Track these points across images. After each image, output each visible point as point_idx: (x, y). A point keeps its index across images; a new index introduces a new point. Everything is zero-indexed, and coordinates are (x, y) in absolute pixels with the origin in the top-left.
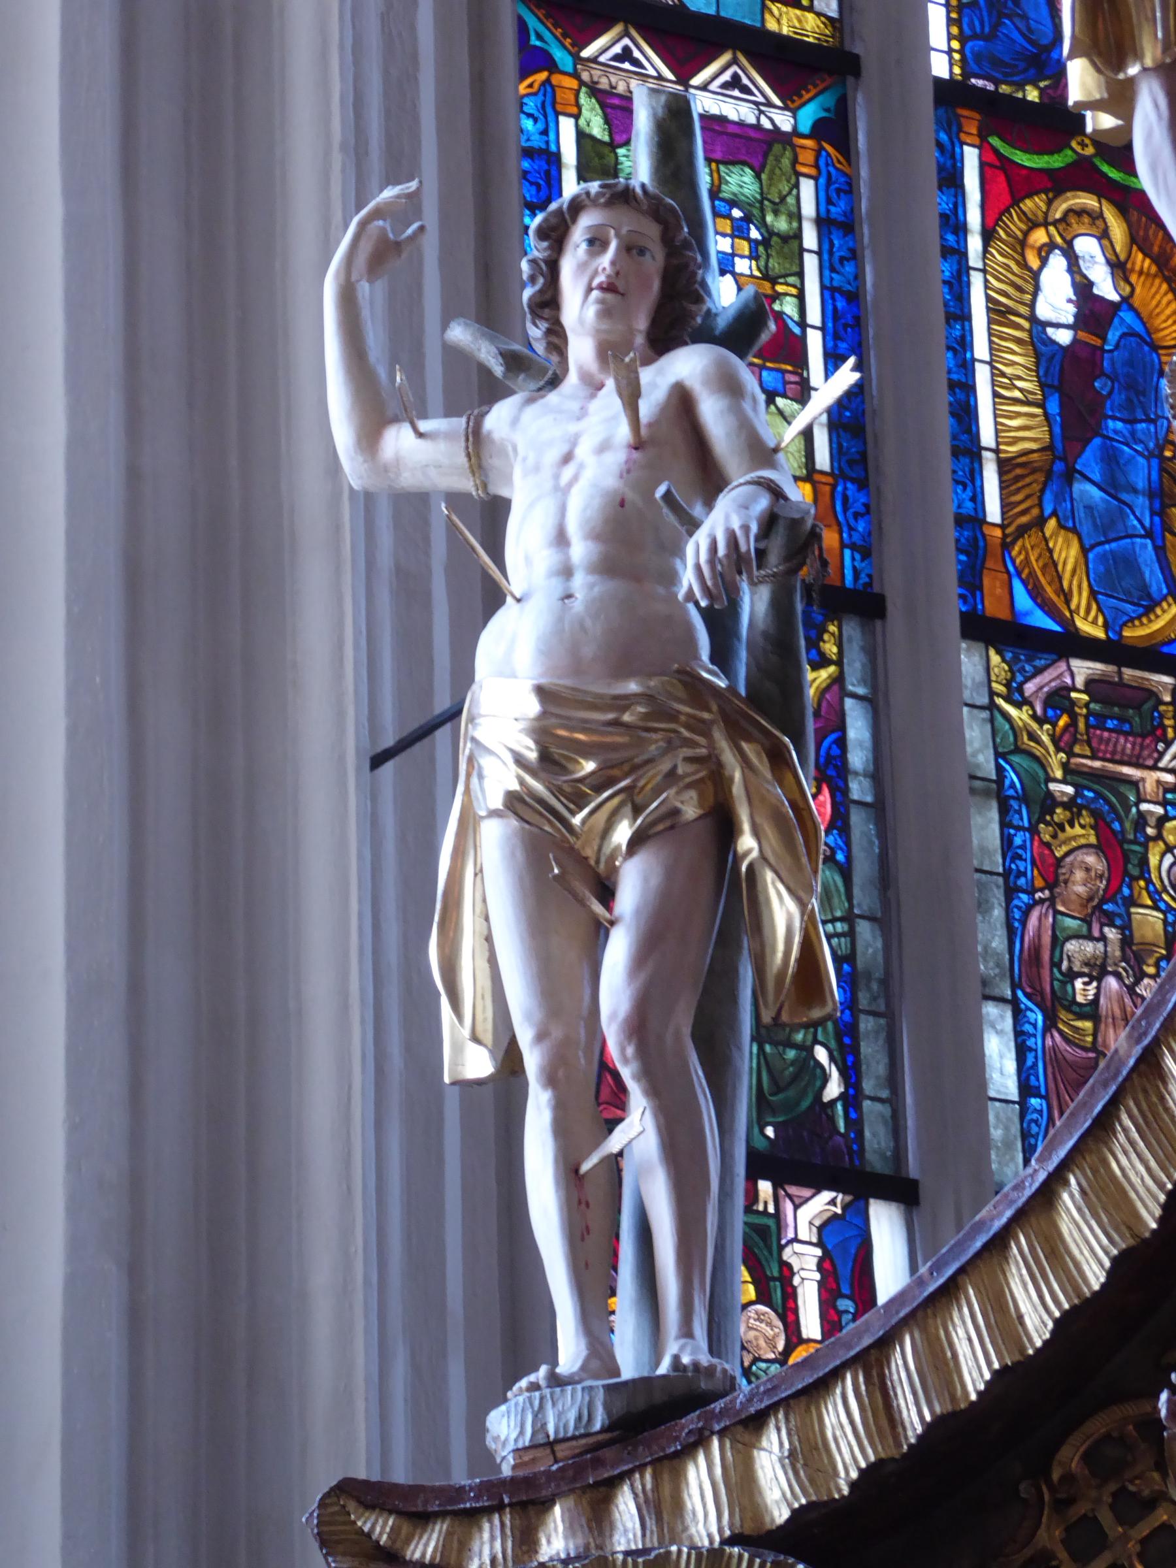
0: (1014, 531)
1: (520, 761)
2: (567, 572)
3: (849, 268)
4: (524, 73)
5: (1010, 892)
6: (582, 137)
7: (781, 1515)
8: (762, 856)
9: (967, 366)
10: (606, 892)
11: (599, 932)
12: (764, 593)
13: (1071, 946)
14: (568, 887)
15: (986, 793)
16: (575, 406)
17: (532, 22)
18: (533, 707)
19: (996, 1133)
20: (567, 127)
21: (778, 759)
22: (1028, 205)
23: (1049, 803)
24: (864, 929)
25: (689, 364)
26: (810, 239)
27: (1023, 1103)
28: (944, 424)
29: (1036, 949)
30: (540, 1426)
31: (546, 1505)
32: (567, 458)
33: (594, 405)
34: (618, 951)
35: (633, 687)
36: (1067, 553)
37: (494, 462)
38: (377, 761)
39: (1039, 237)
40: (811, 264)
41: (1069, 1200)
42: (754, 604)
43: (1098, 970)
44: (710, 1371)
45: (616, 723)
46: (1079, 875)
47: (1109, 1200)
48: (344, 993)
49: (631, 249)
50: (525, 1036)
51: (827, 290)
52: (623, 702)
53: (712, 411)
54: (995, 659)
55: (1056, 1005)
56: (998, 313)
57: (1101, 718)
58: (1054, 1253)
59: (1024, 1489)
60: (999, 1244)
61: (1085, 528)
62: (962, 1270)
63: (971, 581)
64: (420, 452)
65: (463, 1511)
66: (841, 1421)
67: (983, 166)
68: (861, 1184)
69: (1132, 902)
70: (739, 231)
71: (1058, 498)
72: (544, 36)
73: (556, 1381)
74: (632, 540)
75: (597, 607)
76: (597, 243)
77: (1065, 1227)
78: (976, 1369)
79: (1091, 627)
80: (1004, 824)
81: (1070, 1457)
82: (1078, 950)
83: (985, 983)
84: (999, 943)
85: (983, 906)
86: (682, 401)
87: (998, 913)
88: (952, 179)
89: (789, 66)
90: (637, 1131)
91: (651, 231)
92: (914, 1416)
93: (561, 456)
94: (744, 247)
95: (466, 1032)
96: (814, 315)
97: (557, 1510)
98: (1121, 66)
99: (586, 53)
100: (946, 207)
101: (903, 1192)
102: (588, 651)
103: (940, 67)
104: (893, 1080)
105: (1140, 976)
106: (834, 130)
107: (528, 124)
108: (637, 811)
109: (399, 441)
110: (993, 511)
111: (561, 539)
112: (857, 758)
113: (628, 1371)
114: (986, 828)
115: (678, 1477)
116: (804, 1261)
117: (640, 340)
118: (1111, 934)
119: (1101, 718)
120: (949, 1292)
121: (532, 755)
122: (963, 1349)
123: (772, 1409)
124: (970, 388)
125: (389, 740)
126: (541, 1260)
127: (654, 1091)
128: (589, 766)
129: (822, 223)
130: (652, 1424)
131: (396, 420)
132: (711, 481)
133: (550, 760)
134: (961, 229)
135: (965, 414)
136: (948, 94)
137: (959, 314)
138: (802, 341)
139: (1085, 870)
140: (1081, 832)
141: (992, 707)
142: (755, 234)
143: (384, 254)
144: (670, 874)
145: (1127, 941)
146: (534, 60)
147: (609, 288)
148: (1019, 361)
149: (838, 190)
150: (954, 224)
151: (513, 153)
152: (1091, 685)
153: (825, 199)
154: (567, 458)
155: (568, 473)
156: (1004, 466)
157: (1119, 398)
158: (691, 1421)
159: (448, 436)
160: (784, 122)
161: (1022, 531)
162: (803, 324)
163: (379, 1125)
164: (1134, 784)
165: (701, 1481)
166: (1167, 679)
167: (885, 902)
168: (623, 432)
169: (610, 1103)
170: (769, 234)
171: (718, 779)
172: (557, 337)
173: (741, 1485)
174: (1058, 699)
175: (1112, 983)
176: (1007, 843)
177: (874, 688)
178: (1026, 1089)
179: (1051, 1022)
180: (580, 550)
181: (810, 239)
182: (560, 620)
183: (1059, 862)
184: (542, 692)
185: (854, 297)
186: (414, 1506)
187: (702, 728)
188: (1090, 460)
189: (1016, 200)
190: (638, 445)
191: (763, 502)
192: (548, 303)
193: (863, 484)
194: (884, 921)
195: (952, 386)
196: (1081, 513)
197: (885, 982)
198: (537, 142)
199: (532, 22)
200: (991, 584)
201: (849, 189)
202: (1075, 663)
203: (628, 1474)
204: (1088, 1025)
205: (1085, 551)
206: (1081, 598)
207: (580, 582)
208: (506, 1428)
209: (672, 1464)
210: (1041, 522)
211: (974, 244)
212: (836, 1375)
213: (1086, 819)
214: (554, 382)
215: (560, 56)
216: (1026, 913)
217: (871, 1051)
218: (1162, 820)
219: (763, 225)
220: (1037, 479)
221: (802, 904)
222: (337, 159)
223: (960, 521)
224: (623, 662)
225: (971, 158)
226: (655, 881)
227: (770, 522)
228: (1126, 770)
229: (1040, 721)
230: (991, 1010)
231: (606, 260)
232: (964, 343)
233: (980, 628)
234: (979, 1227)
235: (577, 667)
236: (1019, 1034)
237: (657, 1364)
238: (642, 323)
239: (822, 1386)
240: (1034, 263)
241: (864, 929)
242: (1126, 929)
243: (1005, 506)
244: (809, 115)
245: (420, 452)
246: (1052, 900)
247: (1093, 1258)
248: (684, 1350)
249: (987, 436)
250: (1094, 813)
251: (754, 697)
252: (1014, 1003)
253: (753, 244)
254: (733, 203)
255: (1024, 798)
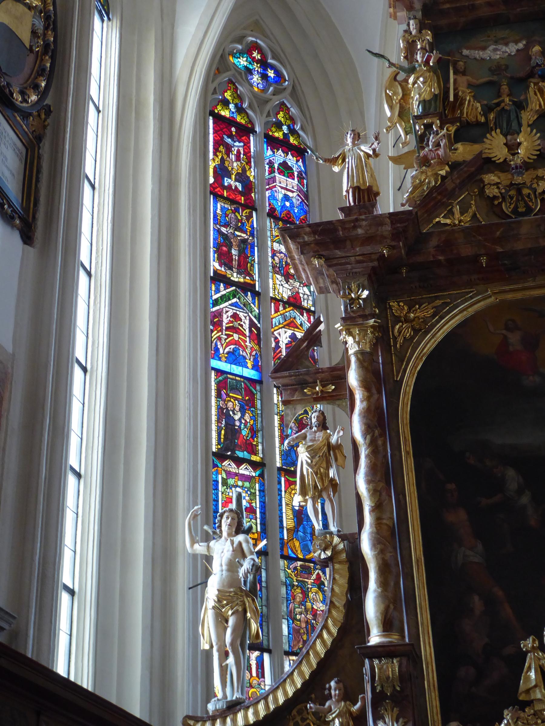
0: (289, 541)
1: (215, 601)
2: (222, 571)
3: (264, 498)
4: (214, 468)
5: (287, 601)
6: (222, 478)
7: (252, 722)
8: (251, 617)
9: (282, 513)
10: (227, 621)
11: (225, 629)
12: (252, 576)
13: (297, 610)
14: (221, 620)
15: (284, 584)
16: (223, 543)
17: (215, 460)
18: (217, 593)
19: (284, 641)
20: (220, 476)
21: (253, 600)
22: (292, 487)
23: (293, 586)
24: (264, 607)
25: (241, 538)
26: (257, 493)
27: (288, 636)
28: (278, 523)
29: (291, 610)
30: (216, 707)
31: (216, 720)
32: (222, 552)
33: (227, 543)
34: (229, 631)
35: (232, 590)
36: (297, 544)
37: (211, 551)
38: (190, 588)
39: (293, 492)
40: (258, 497)
41: (295, 674)
42: (250, 577)
43: (301, 613)
44: (241, 699)
45: (229, 595)
46: (298, 598)
47: (301, 674)
48: (184, 626)
49: (233, 519)
50: (214, 644)
51: (260, 502)
52: (230, 592)
53: (244, 546)
54: (285, 562)
55: (294, 619)
56: (287, 505)
57: (302, 571)
58: (293, 682)
59: (288, 717)
60: (285, 680)
61: (300, 540)
62: (280, 684)
63: (282, 549)
64: (200, 548)
65: (203, 720)
66: (261, 707)
67: (285, 481)
68: (262, 649)
69: (306, 602)
70: (246, 492)
71: (296, 535)
72: (217, 462)
73: (218, 700)
74: (233, 566)
75: (227, 577)
76: (228, 518)
77: (295, 678)
78: (281, 700)
79: (301, 556)
80: (287, 589)
81: (294, 712)
82: (298, 610)
83: (283, 616)
84: (285, 609)
85: (283, 603)
86: (240, 544)
87: (285, 604)
88: (280, 483)
89: (254, 465)
90: (231, 660)
91: (236, 516)
92: (272, 707)
93: (221, 550)
94: (247, 495)
95: (205, 642)
96: (258, 506)
97: (218, 720)
98: (305, 497)
99: (223, 464)
100: (279, 487)
101: (269, 651)
102: (225, 584)
103: (278, 465)
104: (268, 633)
105: (307, 614)
106: (261, 475)
107: (214, 476)
108: (232, 609)
109: (196, 546)
110: (286, 538)
111: (221, 565)
112: (264, 579)
113: (229, 699)
114: (283, 590)
115: (236, 716)
116: (253, 663)
117: (233, 533)
118: (303, 607)
119: (302, 571)
120: (278, 688)
121: (216, 600)
122: (279, 697)
123: (250, 706)
124: (282, 517)
125: (191, 586)
126: (213, 672)
127: (234, 653)
128: (225, 602)
129: (260, 491)
130: (233, 707)
131: (196, 543)
132: (244, 556)
133: (219, 601)
134: (281, 491)
135: (281, 521)
136: (280, 469)
137: (280, 505)
138: (256, 510)
139: (299, 596)
140: (299, 590)
141: (285, 570)
142: (249, 493)
143: (195, 516)
144: (237, 620)
145: (305, 609)
146: (215, 466)
147: (229, 525)
148: (290, 512)
149: (262, 485)
150: (280, 490)
151: (212, 481)
152: (301, 566)
153: (260, 487)
154: (222, 552)
155: (223, 554)
156: (287, 530)
157: (306, 518)
158: (238, 707)
159: (204, 546)
160: (254, 474)
161: (290, 541)
162: (256, 507)
163: (189, 647)
164: (307, 582)
165: (240, 716)
166: (313, 565)
167: (267, 603)
168: (231, 549)
169: (227, 654)
170: (251, 492)
171: (244, 604)
172: (221, 531)
173: (246, 717)
174: (295, 568)
175: (303, 615)
176: (287, 592)
177: (266, 567)
178: (289, 634)
179: (293, 622)
180: (224, 567)
181: (257, 493)
182: (221, 579)
183: (295, 595)
184: (218, 590)
185: (264, 503)
186: (197, 719)
187: (242, 596)
188: (301, 528)
189: (290, 486)
190: (233, 551)
191: (252, 562)
192: (220, 526)
193: (265, 533)
194: (267, 606)
195: (279, 517)
196: (299, 538)
197: (267, 617)
198: (215, 479)
199: (215, 460)
200: (285, 549)
201: (264, 485)
202: (298, 562)
203: (229, 715)
204: (299, 623)
205: (300, 544)
206: (299, 552)
207: (224, 572)
208: (211, 707)
209: (235, 714)
210: (293, 539)
211: (283, 493)
212: (260, 700)
213: (299, 588)
214: (221, 537)
215: (219, 465)
216: (290, 604)
217: (265, 628)
218: (311, 588)
219: (250, 491)
220: (293, 531)
221: (257, 625)
222: (186, 492)
223: (281, 539)
224: (230, 586)
225: (283, 479)
226: (235, 621)
227: (253, 565)
228: (306, 580)
229: (292, 572)
230: (284, 620)
231: (229, 520)
232: (281, 510)
233: (283, 557)
234: (282, 678)
235: (223, 586)
236: (288, 624)
237: (233, 696)
238: (234, 530)
239: (258, 702)
240: (292, 496)
241: (264, 607)
242: (305, 606)
243: (288, 537)
244: (258, 473)
245: (200, 548)
246: (294, 602)
247: (299, 683)
248: (237, 695)
249: (285, 525)
250: (301, 588)
251: (250, 591)
252: (287, 619)
253: (249, 494)
254: (245, 488)
255: (290, 585)
